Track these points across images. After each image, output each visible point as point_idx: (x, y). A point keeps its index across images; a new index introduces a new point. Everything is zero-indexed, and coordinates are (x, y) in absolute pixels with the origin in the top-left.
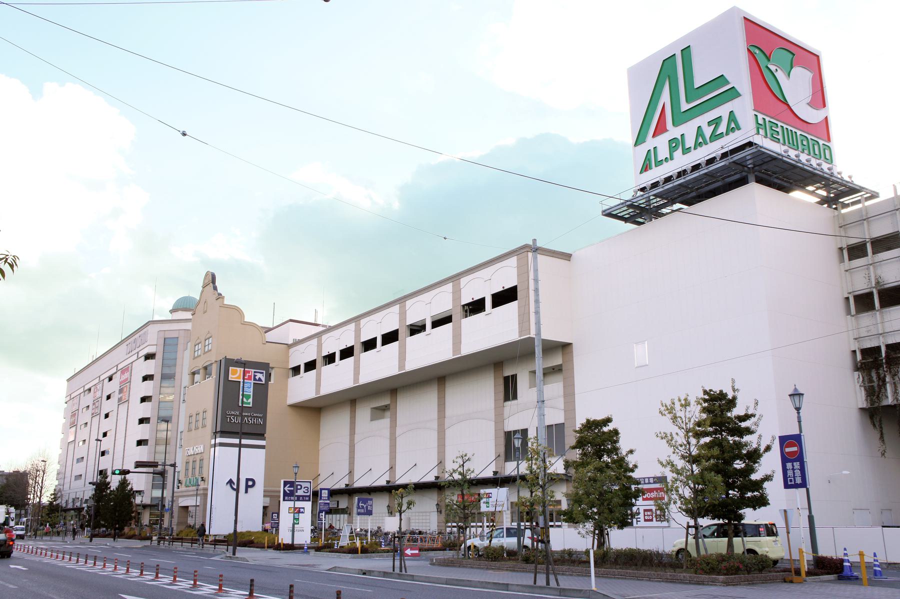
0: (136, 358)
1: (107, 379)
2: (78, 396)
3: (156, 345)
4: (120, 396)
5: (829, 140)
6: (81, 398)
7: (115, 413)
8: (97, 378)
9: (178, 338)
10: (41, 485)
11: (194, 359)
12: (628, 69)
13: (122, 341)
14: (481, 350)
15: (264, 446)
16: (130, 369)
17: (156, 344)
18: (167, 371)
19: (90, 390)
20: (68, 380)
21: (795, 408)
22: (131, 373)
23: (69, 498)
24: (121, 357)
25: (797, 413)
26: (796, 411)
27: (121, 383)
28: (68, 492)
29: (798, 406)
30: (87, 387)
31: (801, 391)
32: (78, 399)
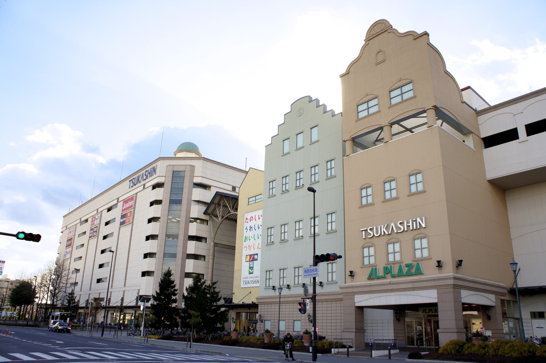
0: (65, 229)
1: (106, 210)
2: (75, 226)
3: (165, 176)
4: (122, 220)
5: (236, 209)
6: (77, 227)
7: (116, 234)
8: (79, 219)
9: (185, 171)
10: (55, 287)
11: (356, 121)
12: (38, 242)
13: (92, 199)
14: (495, 178)
15: (186, 277)
16: (134, 198)
17: (165, 175)
18: (175, 198)
19: (86, 221)
20: (64, 217)
21: (513, 271)
22: (136, 201)
23: (80, 298)
24: (125, 192)
25: (514, 273)
26: (514, 272)
27: (123, 210)
28: (80, 293)
29: (515, 270)
30: (83, 219)
31: (516, 261)
32: (74, 228)
